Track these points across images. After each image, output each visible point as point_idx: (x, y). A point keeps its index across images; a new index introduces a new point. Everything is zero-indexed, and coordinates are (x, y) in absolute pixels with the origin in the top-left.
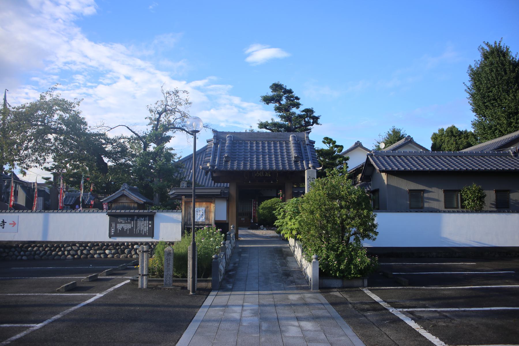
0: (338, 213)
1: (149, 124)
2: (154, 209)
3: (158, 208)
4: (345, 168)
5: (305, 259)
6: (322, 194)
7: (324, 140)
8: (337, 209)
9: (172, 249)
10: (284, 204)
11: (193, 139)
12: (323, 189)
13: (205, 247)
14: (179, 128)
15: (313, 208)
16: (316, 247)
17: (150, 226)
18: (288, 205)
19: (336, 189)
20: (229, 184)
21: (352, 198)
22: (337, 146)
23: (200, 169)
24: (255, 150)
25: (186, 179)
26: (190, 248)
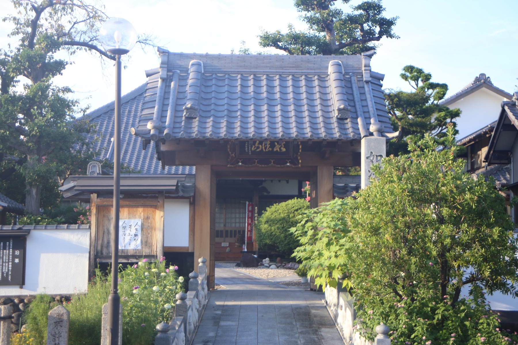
0: (433, 233)
1: (13, 34)
2: (26, 224)
3: (35, 220)
4: (450, 134)
5: (360, 334)
6: (397, 191)
7: (403, 72)
8: (431, 223)
9: (65, 311)
10: (315, 213)
11: (114, 69)
12: (400, 179)
13: (141, 306)
14: (84, 44)
15: (378, 220)
16: (384, 308)
17: (17, 261)
18: (324, 215)
19: (430, 179)
20: (194, 167)
21: (466, 200)
22: (433, 86)
23: (131, 135)
24: (252, 93)
25: (101, 157)
26: (107, 308)
